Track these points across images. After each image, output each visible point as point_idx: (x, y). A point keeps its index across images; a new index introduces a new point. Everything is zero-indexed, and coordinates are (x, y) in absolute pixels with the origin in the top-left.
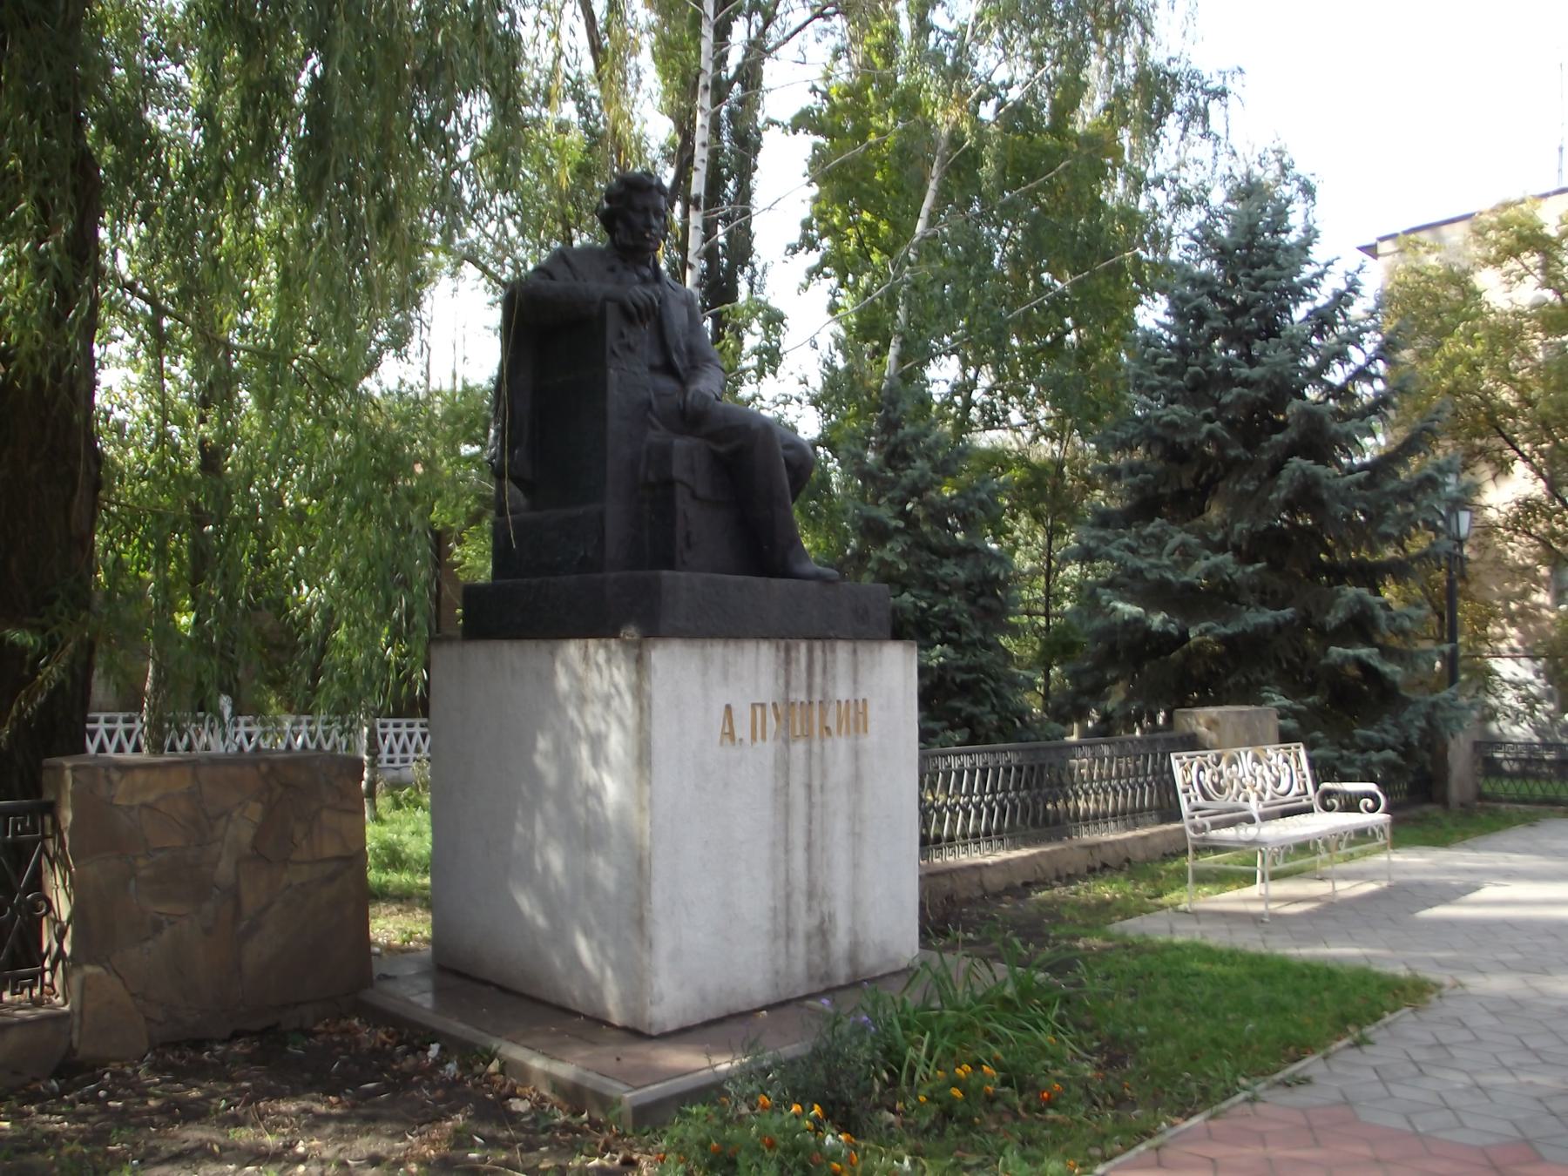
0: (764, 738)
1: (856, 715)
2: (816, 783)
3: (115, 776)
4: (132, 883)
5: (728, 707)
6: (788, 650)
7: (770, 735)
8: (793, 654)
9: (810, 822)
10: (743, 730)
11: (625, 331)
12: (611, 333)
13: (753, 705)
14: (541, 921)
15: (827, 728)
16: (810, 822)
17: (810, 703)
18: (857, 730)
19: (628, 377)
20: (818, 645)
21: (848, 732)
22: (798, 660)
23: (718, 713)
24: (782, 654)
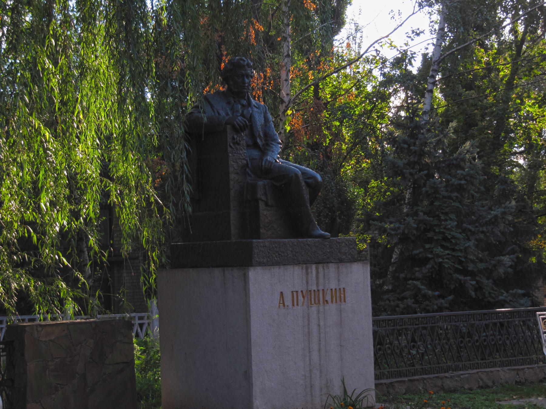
0: (297, 305)
1: (339, 296)
2: (322, 324)
3: (40, 329)
4: (47, 372)
5: (282, 293)
6: (307, 269)
7: (300, 304)
8: (309, 271)
9: (320, 334)
10: (288, 302)
11: (235, 137)
12: (229, 137)
13: (292, 292)
14: (461, 268)
15: (327, 301)
16: (320, 334)
17: (318, 290)
18: (341, 301)
19: (239, 156)
20: (320, 266)
21: (336, 302)
22: (312, 272)
23: (277, 296)
24: (304, 271)
